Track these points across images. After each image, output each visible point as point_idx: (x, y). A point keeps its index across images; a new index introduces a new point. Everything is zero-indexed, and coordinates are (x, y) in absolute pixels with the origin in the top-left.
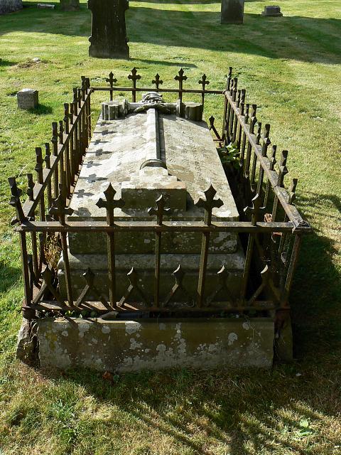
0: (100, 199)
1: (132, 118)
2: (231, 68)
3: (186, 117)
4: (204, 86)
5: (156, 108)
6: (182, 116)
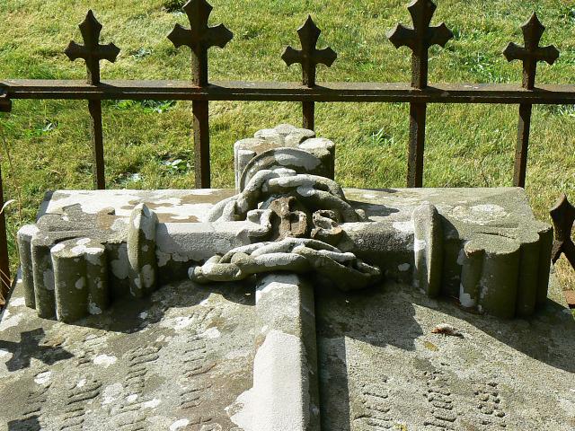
0: (177, 26)
1: (178, 320)
2: (426, 424)
3: (465, 299)
4: (530, 71)
5: (306, 273)
6: (443, 294)
